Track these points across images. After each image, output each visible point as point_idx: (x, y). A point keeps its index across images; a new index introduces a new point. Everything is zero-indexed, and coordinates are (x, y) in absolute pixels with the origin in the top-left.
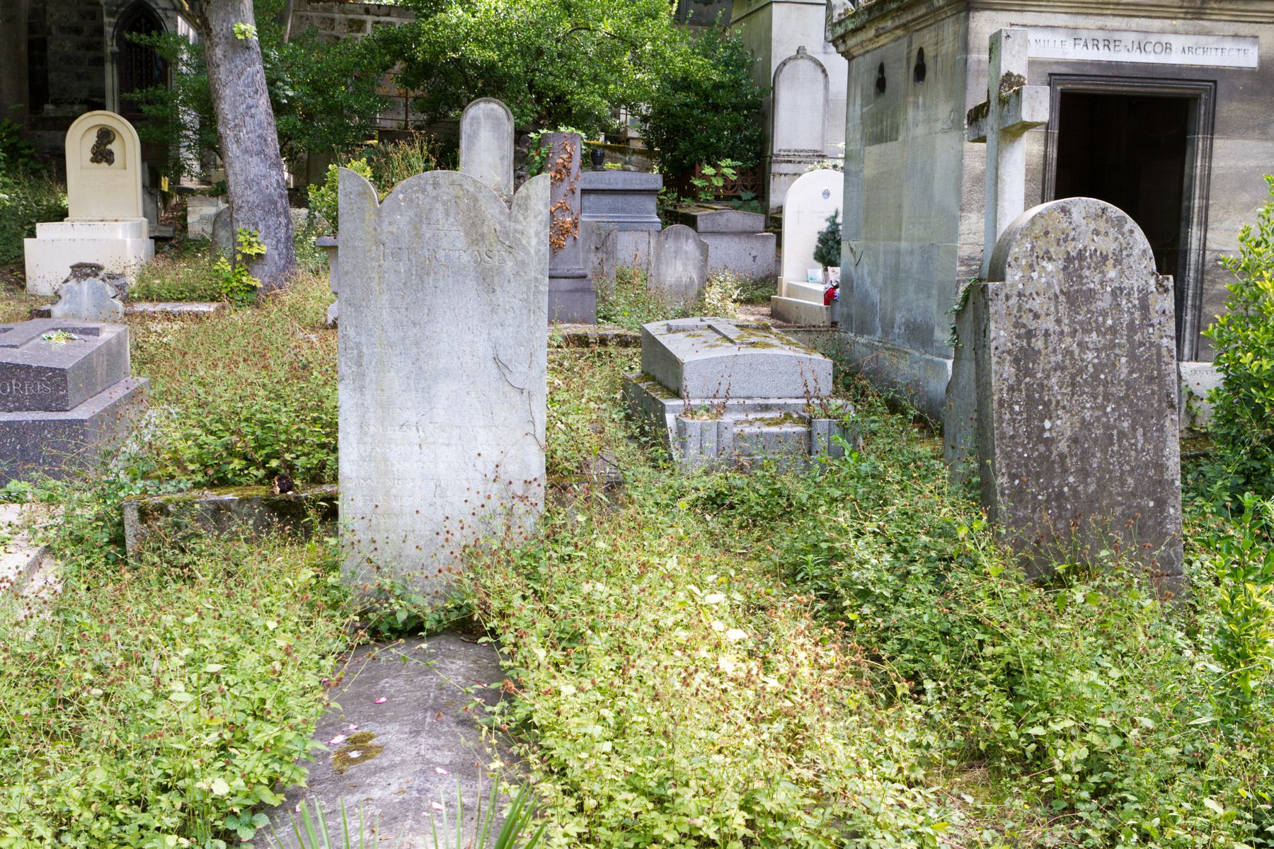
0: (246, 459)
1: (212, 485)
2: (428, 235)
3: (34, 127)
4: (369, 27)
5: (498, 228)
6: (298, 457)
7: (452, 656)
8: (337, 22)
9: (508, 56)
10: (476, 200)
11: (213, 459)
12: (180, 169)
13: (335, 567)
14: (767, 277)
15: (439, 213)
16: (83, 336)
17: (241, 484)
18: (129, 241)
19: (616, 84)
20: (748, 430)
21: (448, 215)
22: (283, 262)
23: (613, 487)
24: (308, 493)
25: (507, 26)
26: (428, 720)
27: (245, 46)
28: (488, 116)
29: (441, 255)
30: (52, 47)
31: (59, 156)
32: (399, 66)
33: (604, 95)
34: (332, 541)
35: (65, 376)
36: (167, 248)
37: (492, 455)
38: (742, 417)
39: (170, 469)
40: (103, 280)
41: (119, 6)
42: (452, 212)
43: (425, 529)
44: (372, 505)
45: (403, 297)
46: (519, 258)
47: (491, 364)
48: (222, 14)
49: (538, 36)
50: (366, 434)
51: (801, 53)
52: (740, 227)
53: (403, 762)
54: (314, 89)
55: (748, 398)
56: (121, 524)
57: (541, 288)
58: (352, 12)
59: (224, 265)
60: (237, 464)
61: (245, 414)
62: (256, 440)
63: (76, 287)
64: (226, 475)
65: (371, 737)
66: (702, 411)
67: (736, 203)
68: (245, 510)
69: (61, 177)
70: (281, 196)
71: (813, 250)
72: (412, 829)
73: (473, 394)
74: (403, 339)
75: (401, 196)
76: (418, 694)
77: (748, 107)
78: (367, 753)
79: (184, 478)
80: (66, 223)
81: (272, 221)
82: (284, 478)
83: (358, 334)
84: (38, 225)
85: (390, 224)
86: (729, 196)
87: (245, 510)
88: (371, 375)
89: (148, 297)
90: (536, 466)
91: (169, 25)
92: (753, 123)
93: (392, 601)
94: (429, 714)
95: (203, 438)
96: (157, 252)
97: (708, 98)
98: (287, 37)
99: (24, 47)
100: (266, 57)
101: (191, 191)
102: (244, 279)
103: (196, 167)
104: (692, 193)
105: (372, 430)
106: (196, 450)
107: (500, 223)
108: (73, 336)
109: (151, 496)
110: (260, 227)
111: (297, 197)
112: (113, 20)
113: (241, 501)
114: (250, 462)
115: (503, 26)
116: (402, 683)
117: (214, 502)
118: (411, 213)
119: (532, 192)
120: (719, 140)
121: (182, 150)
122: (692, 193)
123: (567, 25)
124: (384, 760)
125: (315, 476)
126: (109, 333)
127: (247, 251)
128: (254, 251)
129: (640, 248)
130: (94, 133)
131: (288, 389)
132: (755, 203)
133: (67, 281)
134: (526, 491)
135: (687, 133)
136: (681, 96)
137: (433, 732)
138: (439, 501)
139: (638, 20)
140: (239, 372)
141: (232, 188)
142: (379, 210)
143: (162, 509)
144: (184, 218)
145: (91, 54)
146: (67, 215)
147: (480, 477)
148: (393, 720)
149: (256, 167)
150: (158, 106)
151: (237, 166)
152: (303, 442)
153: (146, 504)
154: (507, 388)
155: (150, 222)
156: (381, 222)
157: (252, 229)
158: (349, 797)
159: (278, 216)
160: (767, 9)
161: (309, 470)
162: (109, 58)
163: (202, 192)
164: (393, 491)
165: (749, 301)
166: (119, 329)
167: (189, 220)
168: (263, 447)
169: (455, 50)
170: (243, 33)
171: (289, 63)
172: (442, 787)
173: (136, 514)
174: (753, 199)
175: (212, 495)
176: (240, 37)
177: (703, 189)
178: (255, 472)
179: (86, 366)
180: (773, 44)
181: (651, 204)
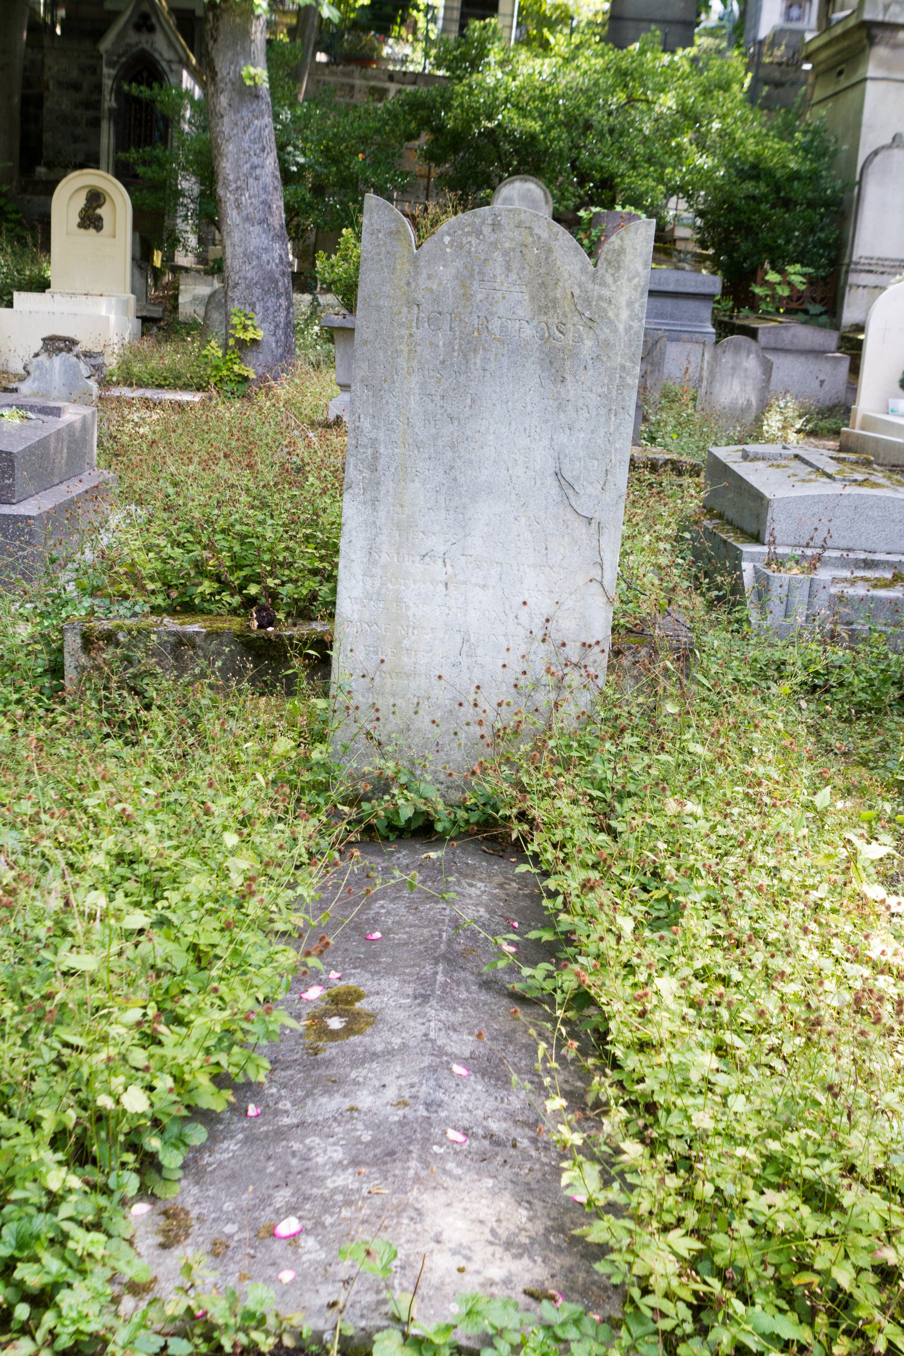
0: (219, 580)
1: (172, 611)
2: (479, 296)
3: (24, 190)
4: (391, 95)
5: (577, 292)
6: (283, 584)
7: (469, 874)
8: (356, 89)
9: (551, 128)
10: (550, 251)
11: (178, 578)
12: (173, 242)
13: (322, 738)
14: (835, 406)
15: (497, 267)
16: (41, 416)
17: (210, 612)
18: (112, 317)
19: (674, 167)
20: (851, 591)
21: (509, 269)
22: (280, 351)
23: (685, 656)
24: (294, 632)
25: (553, 93)
26: (440, 978)
27: (253, 94)
28: (524, 197)
30: (48, 104)
31: (45, 221)
32: (424, 139)
33: (660, 180)
34: (321, 703)
35: (12, 461)
36: (155, 330)
37: (542, 605)
38: (846, 573)
39: (125, 587)
40: (77, 356)
41: (119, 56)
42: (515, 265)
43: (443, 696)
44: (376, 659)
45: (439, 381)
46: (602, 337)
47: (551, 481)
48: (230, 55)
49: (588, 105)
50: (375, 563)
52: (808, 345)
53: (404, 1047)
54: (328, 158)
55: (849, 550)
56: (60, 650)
57: (629, 380)
58: (374, 78)
59: (214, 349)
60: (207, 587)
61: (221, 523)
62: (233, 558)
63: (47, 363)
64: (192, 600)
65: (359, 997)
66: (793, 564)
67: (801, 316)
68: (212, 647)
69: (46, 246)
70: (283, 274)
72: (417, 1179)
73: (523, 520)
74: (435, 438)
75: (447, 239)
76: (426, 931)
77: (827, 204)
78: (356, 1023)
79: (140, 600)
80: (46, 295)
81: (271, 302)
82: (263, 608)
83: (375, 427)
84: (16, 294)
85: (429, 277)
86: (795, 307)
87: (212, 647)
88: (388, 485)
89: (129, 380)
90: (599, 624)
91: (173, 80)
92: (830, 224)
93: (395, 791)
94: (440, 968)
95: (168, 550)
96: (143, 334)
97: (780, 190)
98: (301, 97)
99: (16, 100)
100: (276, 117)
101: (187, 270)
102: (236, 368)
103: (193, 241)
104: (752, 302)
105: (384, 558)
106: (159, 566)
107: (580, 285)
108: (30, 415)
109: (99, 619)
110: (258, 308)
111: (303, 281)
112: (113, 72)
113: (209, 635)
114: (224, 585)
115: (549, 91)
116: (403, 911)
117: (175, 634)
118: (459, 263)
119: (628, 243)
120: (788, 242)
121: (179, 221)
122: (752, 302)
123: (621, 97)
124: (377, 1039)
125: (303, 610)
126: (72, 414)
127: (241, 335)
128: (249, 336)
129: (692, 359)
130: (83, 195)
131: (277, 496)
132: (824, 319)
133: (36, 355)
134: (584, 656)
135: (749, 230)
136: (749, 186)
137: (448, 1001)
138: (465, 661)
139: (706, 92)
140: (218, 470)
141: (229, 262)
142: (416, 258)
143: (110, 637)
144: (176, 297)
145: (90, 114)
146: (49, 286)
147: (523, 633)
148: (390, 970)
149: (257, 238)
150: (155, 167)
151: (236, 236)
152: (291, 564)
153: (91, 629)
154: (570, 515)
155: (138, 300)
156: (417, 274)
157: (248, 310)
158: (324, 1100)
159: (279, 296)
161: (296, 601)
162: (106, 114)
163: (198, 271)
164: (406, 643)
165: (812, 433)
166: (87, 411)
167: (181, 300)
168: (241, 568)
169: (490, 118)
170: (253, 78)
171: (300, 123)
172: (462, 1098)
173: (79, 640)
174: (821, 314)
175: (171, 624)
176: (249, 82)
177: (763, 299)
179: (40, 451)
180: (864, 130)
181: (705, 311)
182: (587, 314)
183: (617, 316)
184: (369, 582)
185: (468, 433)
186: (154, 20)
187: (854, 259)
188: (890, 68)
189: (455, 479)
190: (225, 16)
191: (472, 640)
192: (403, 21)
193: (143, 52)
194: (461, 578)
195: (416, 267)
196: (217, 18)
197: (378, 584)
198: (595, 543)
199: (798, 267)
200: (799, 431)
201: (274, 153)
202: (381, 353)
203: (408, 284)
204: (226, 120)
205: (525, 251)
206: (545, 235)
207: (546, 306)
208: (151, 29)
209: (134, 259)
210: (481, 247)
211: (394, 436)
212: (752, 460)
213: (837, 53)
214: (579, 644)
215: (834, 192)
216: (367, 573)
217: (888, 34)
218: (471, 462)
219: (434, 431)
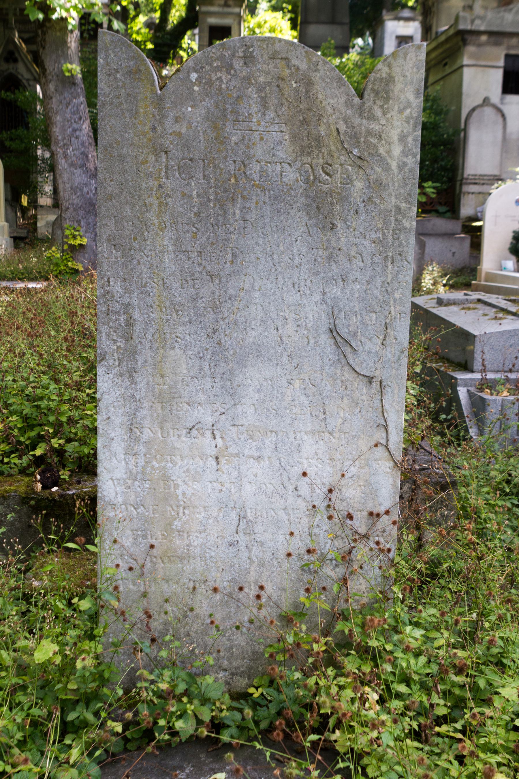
2: (234, 139)
5: (343, 128)
10: (310, 83)
15: (252, 103)
21: (265, 105)
29: (254, 169)
37: (323, 474)
42: (272, 101)
44: (144, 544)
46: (373, 177)
47: (325, 339)
48: (54, 57)
50: (137, 440)
51: (486, 101)
57: (406, 223)
62: (25, 418)
67: (434, 214)
71: (508, 245)
74: (195, 299)
75: (194, 76)
83: (126, 290)
85: (177, 120)
88: (146, 354)
90: (387, 488)
102: (70, 264)
105: (147, 433)
107: (346, 120)
110: (82, 223)
118: (208, 103)
119: (396, 71)
127: (72, 242)
128: (78, 242)
132: (448, 214)
138: (242, 539)
144: (35, 223)
147: (302, 505)
151: (65, 176)
154: (348, 375)
155: (10, 226)
156: (163, 116)
160: (459, 72)
164: (177, 524)
167: (39, 225)
168: (32, 427)
170: (70, 71)
176: (67, 74)
178: (16, 461)
180: (464, 97)
182: (356, 152)
183: (389, 152)
184: (132, 461)
185: (231, 291)
186: (17, 55)
187: (465, 176)
188: (477, 58)
189: (220, 343)
190: (49, 31)
191: (249, 516)
192: (174, 58)
193: (11, 74)
194: (232, 450)
195: (161, 109)
196: (44, 33)
197: (141, 463)
198: (378, 404)
199: (430, 183)
200: (444, 285)
201: (88, 121)
202: (128, 208)
203: (154, 129)
204: (54, 100)
205: (283, 85)
206: (303, 66)
207: (310, 146)
208: (15, 61)
209: (6, 200)
210: (233, 83)
211: (149, 300)
212: (446, 305)
213: (442, 53)
214: (365, 514)
215: (448, 136)
216: (129, 452)
217: (474, 38)
218: (236, 323)
219: (192, 291)
